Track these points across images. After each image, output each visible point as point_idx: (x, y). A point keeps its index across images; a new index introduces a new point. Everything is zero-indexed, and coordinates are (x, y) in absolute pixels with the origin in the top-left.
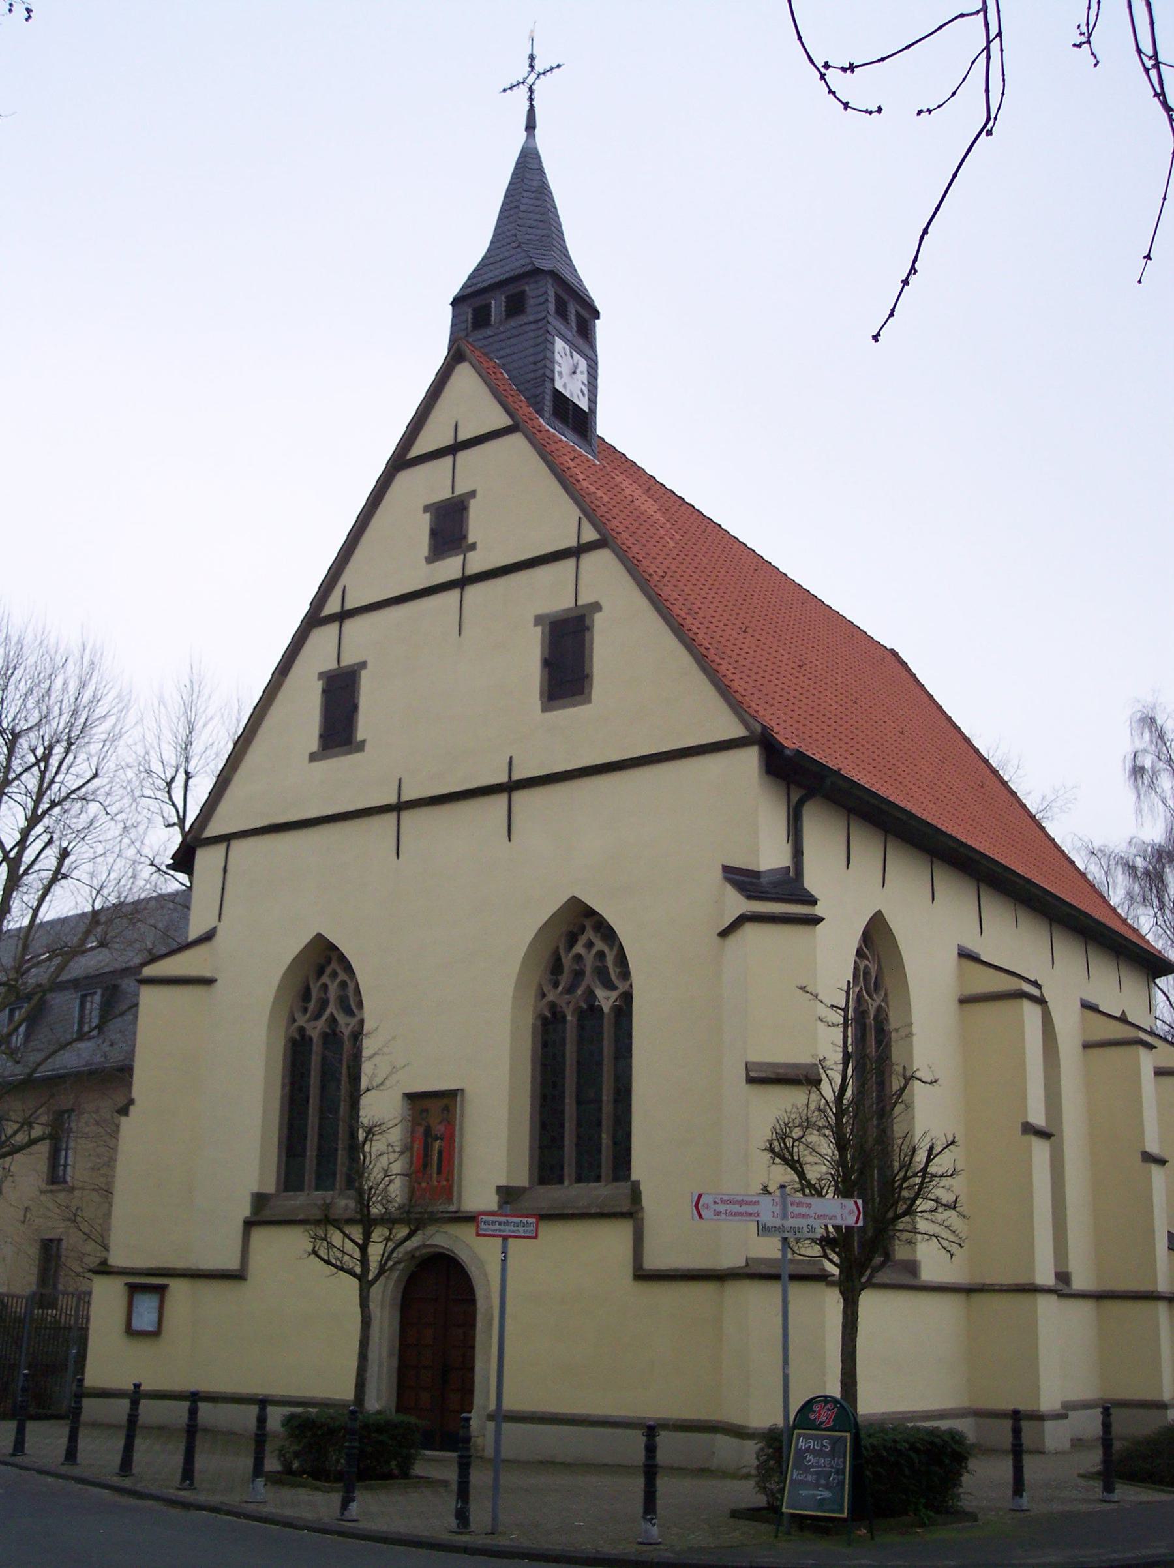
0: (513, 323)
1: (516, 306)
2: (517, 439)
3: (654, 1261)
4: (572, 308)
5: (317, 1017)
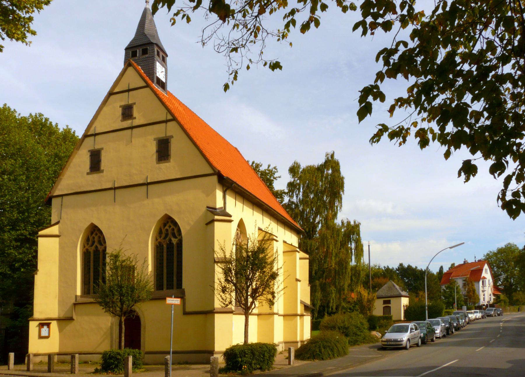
0: (144, 57)
1: (145, 52)
2: (147, 89)
3: (188, 310)
4: (161, 54)
5: (92, 246)
